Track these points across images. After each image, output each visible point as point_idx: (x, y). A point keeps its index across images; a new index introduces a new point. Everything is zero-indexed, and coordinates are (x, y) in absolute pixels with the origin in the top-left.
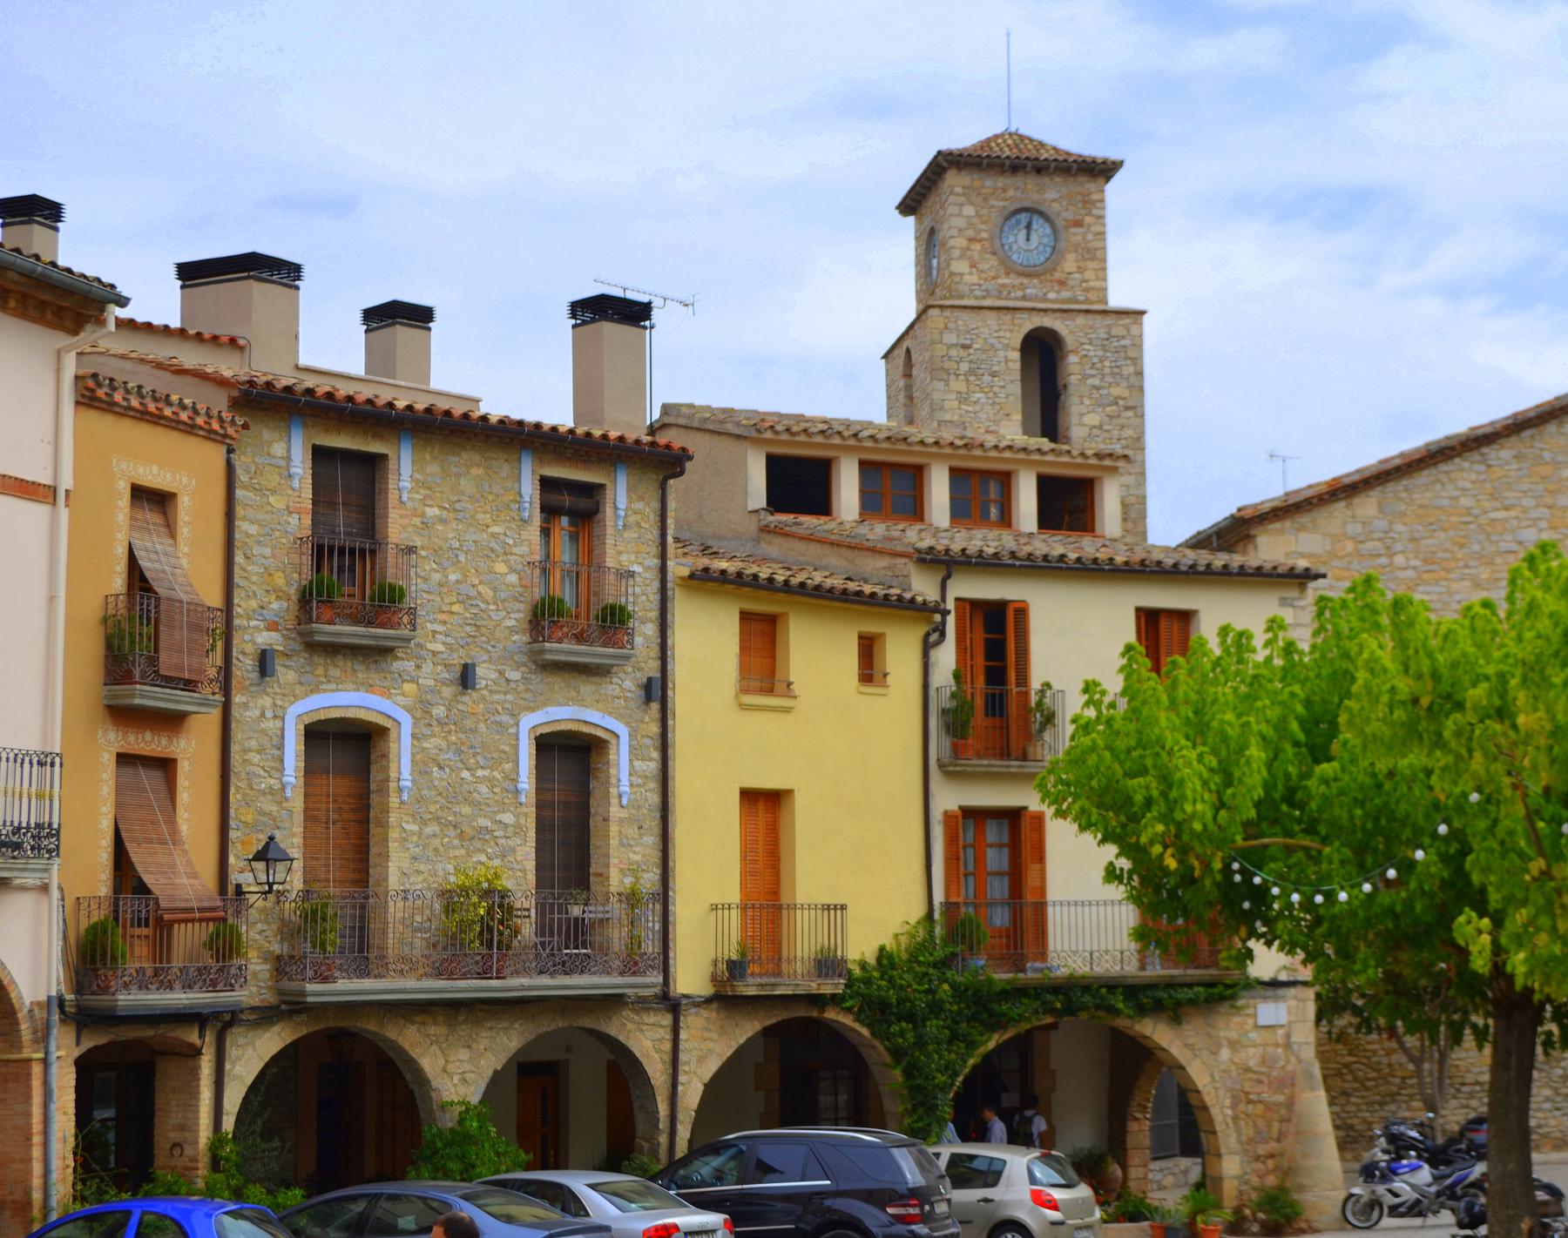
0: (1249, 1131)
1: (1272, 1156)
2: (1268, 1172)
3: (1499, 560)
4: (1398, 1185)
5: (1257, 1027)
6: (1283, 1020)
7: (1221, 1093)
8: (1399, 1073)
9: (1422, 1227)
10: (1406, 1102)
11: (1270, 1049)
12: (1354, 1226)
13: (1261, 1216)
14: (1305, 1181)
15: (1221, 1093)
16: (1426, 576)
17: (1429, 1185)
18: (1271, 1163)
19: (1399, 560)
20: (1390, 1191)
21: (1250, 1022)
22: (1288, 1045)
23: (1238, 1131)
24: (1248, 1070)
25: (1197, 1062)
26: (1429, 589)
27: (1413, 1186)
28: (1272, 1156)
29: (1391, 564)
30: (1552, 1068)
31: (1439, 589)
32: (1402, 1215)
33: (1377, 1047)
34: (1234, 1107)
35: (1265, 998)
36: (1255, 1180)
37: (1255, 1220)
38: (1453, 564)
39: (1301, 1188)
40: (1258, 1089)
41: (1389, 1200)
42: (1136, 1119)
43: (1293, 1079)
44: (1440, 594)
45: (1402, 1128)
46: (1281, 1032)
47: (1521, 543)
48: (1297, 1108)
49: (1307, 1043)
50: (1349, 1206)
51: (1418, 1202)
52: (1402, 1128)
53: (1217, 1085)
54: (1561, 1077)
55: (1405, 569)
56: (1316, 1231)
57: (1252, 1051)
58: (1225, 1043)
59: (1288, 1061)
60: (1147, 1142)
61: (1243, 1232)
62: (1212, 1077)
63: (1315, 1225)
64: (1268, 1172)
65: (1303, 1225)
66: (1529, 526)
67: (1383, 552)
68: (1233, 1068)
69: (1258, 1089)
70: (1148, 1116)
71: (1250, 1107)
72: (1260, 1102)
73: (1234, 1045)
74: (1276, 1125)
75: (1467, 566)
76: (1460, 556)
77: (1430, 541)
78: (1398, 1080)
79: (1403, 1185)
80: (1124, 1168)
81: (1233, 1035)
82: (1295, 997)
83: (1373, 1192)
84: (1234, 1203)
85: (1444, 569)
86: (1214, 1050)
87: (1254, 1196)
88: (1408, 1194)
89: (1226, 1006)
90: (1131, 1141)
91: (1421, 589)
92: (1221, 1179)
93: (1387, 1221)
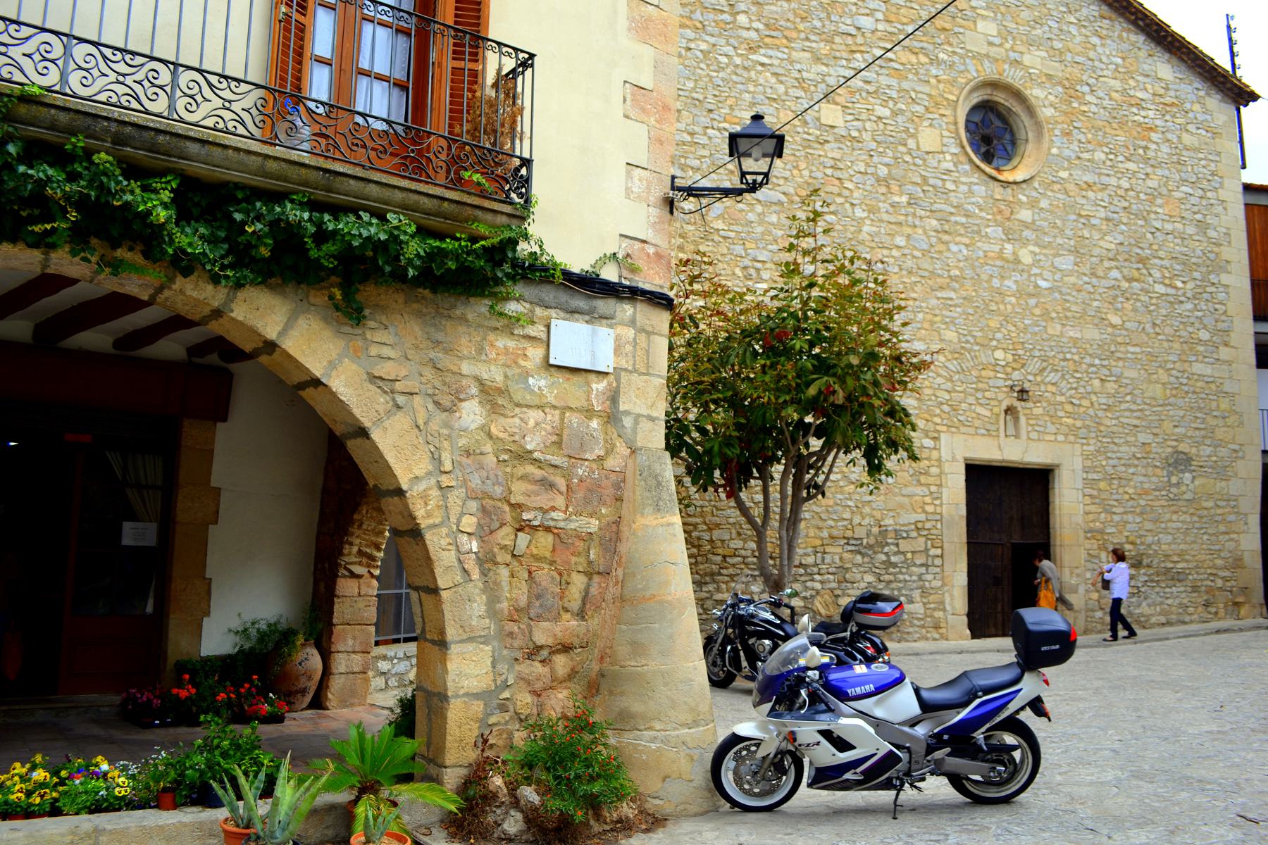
0: (514, 591)
1: (566, 648)
2: (556, 682)
3: (837, 39)
4: (847, 724)
5: (548, 366)
6: (605, 361)
7: (455, 498)
8: (720, 551)
9: (895, 810)
10: (726, 583)
11: (574, 419)
12: (734, 803)
13: (529, 794)
14: (637, 707)
15: (455, 498)
16: (767, 40)
17: (913, 723)
18: (561, 663)
19: (742, 19)
20: (827, 734)
21: (536, 353)
22: (612, 417)
23: (492, 590)
24: (523, 456)
25: (400, 422)
26: (770, 52)
27: (879, 724)
28: (566, 648)
29: (734, 22)
30: (875, 553)
31: (780, 55)
32: (847, 786)
33: (698, 520)
34: (484, 533)
35: (572, 312)
36: (524, 700)
37: (516, 803)
38: (794, 35)
39: (625, 720)
40: (543, 500)
41: (828, 755)
42: (353, 575)
43: (617, 487)
44: (782, 60)
45: (752, 608)
46: (599, 386)
47: (859, 29)
48: (623, 548)
49: (652, 419)
50: (729, 763)
51: (889, 760)
52: (752, 608)
53: (445, 480)
54: (884, 562)
55: (748, 29)
56: (655, 822)
57: (533, 416)
58: (474, 390)
59: (610, 450)
60: (372, 614)
61: (485, 834)
62: (437, 460)
63: (652, 804)
64: (556, 682)
65: (627, 810)
66: (868, 15)
67: (726, 9)
68: (488, 448)
69: (543, 500)
70: (377, 572)
71: (523, 538)
72: (548, 529)
73: (492, 396)
74: (579, 581)
75: (807, 39)
76: (801, 27)
77: (773, 8)
78: (719, 558)
79: (859, 722)
80: (326, 655)
81: (495, 375)
82: (632, 323)
83: (792, 737)
84: (472, 755)
85: (786, 38)
86: (446, 401)
87: (520, 737)
88: (869, 744)
89: (479, 308)
90: (341, 610)
91: (762, 51)
92: (444, 697)
93: (807, 796)
